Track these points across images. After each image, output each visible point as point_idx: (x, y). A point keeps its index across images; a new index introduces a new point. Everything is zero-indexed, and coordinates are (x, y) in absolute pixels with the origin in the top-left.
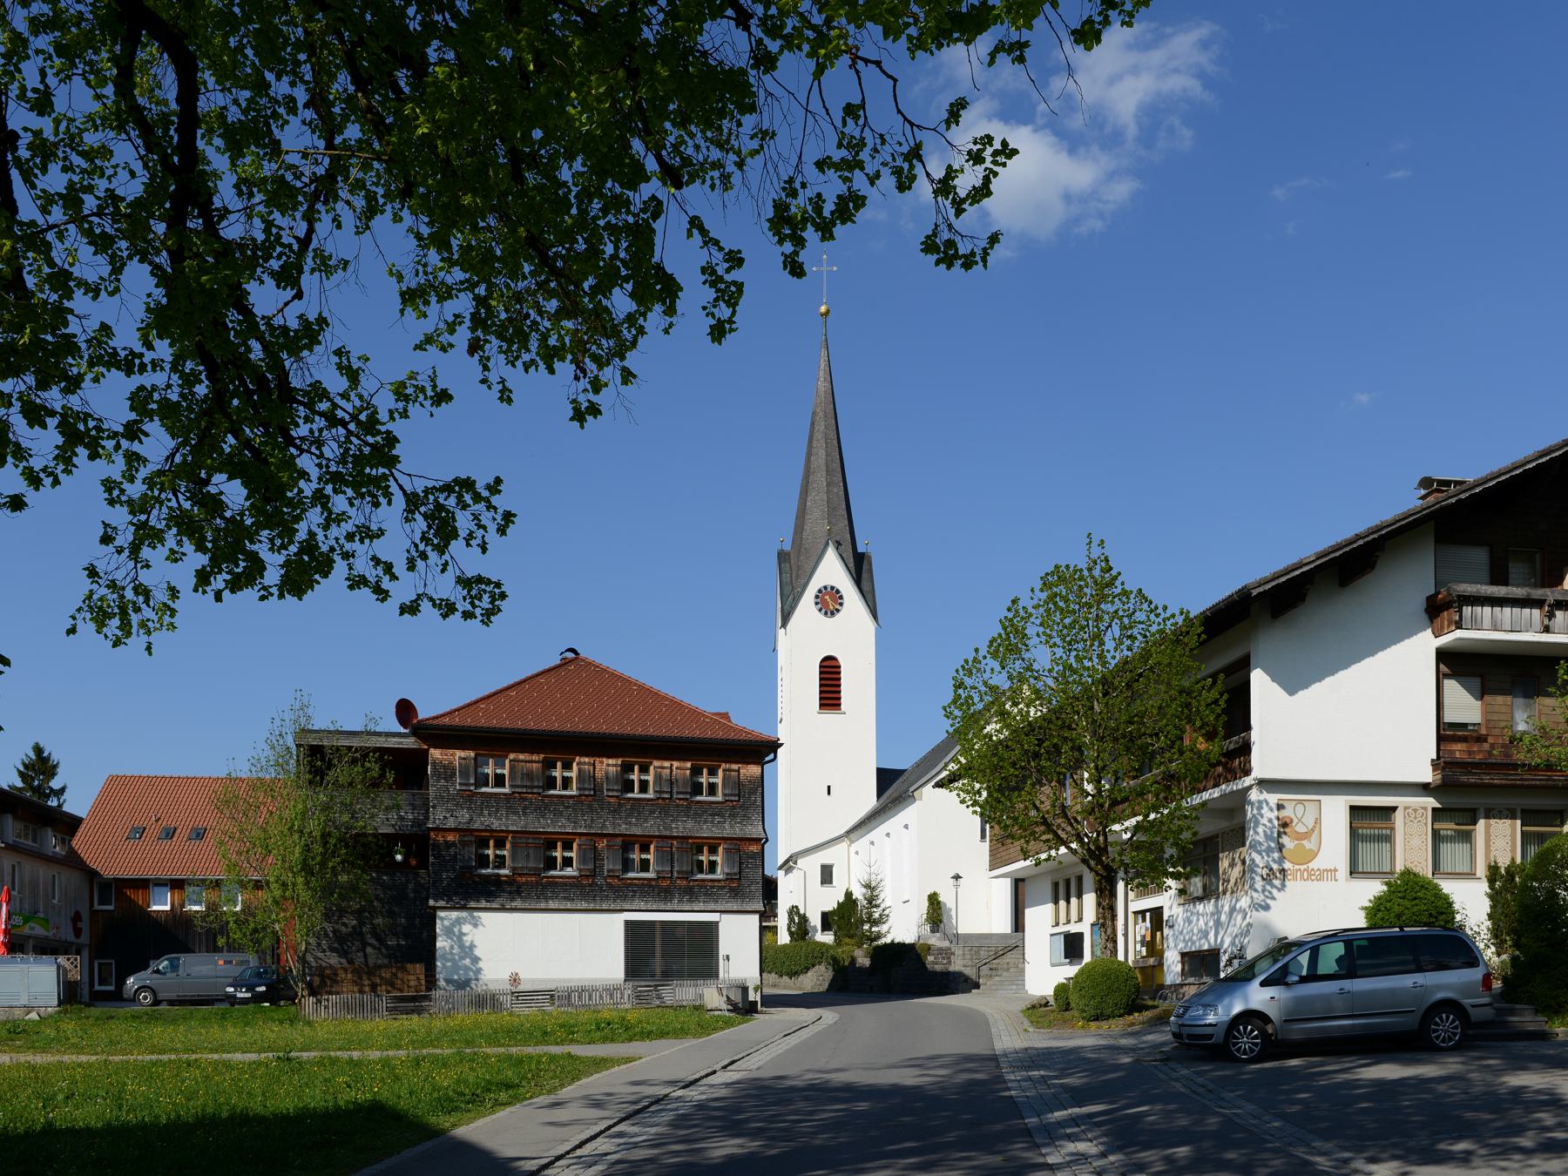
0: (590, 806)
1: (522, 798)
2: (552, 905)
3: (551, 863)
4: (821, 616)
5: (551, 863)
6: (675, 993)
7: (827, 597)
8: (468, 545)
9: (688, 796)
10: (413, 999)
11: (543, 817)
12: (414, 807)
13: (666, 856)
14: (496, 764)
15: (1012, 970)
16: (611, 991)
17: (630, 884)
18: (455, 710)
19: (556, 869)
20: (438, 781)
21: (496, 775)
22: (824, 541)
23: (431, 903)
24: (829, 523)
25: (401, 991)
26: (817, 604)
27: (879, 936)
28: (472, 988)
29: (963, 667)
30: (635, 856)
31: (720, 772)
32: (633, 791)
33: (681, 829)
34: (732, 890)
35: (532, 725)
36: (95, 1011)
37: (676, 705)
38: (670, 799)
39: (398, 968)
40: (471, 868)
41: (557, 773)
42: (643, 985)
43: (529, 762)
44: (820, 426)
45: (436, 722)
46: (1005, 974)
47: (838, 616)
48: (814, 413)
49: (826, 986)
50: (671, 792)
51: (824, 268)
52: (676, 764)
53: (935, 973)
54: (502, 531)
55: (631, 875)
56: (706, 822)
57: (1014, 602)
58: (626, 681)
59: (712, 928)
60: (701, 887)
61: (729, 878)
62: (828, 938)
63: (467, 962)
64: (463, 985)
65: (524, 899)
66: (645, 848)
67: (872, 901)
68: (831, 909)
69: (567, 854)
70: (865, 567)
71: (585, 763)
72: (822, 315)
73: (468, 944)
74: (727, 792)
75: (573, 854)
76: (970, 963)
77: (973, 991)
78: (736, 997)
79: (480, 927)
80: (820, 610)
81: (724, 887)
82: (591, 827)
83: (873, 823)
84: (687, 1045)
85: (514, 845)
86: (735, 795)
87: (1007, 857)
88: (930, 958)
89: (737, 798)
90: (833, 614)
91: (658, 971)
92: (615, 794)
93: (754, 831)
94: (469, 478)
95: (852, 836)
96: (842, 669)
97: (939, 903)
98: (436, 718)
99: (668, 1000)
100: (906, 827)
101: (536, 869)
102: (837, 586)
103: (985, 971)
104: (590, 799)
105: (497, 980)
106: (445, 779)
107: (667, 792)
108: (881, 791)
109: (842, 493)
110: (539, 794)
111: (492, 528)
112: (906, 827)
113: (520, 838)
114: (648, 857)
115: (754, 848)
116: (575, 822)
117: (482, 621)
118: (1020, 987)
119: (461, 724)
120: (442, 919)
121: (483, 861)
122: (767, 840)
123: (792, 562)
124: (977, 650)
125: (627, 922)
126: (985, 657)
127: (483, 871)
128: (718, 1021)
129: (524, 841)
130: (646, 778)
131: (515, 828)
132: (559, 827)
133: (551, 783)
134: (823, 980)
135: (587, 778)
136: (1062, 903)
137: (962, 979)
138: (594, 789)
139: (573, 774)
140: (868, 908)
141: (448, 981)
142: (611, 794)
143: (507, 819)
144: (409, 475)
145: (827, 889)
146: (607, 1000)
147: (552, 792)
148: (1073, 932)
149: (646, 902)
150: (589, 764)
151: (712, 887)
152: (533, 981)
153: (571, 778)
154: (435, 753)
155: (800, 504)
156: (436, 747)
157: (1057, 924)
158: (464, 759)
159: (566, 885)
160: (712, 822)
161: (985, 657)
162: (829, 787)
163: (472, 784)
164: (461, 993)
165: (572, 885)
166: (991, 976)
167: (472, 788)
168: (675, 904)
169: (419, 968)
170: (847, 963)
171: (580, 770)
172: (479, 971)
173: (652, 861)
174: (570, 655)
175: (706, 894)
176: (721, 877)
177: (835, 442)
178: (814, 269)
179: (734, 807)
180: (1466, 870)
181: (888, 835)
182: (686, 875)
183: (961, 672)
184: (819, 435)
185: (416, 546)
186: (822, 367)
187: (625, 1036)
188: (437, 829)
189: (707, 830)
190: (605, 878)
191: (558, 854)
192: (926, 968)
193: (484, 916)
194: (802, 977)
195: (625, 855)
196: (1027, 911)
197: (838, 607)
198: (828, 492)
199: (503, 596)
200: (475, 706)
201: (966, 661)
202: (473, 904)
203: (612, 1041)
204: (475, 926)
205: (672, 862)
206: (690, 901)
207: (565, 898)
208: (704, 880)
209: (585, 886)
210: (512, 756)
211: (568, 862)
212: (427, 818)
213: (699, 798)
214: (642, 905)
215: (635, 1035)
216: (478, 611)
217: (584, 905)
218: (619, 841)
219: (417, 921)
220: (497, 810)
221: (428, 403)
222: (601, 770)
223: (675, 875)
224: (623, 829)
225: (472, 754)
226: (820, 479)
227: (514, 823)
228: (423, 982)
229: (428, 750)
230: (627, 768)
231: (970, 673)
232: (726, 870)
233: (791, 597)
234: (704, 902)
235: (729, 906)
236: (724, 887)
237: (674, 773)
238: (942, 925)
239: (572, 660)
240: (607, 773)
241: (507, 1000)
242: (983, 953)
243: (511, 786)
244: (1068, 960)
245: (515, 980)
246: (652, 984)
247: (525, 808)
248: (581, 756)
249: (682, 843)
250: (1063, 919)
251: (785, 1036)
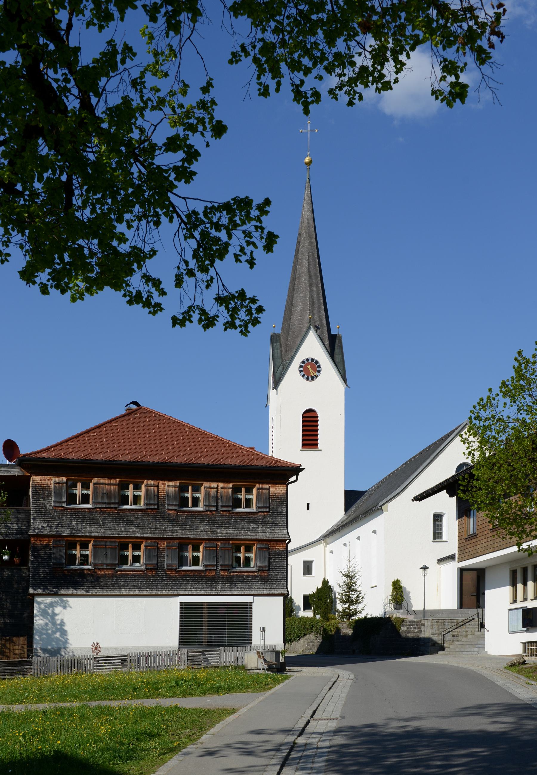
0: (155, 517)
1: (102, 512)
2: (124, 591)
3: (123, 560)
4: (303, 380)
5: (123, 560)
6: (220, 657)
7: (309, 367)
8: (238, 260)
9: (230, 509)
10: (20, 663)
11: (118, 525)
12: (18, 519)
13: (213, 554)
14: (82, 487)
15: (469, 636)
16: (170, 656)
17: (184, 575)
18: (51, 447)
19: (127, 564)
20: (38, 499)
21: (82, 494)
22: (306, 326)
23: (31, 591)
24: (311, 313)
25: (8, 657)
26: (301, 371)
27: (355, 613)
28: (61, 655)
29: (479, 403)
30: (188, 554)
31: (255, 491)
32: (187, 506)
33: (224, 534)
34: (263, 578)
35: (111, 457)
36: (215, 709)
37: (219, 442)
38: (216, 511)
39: (7, 641)
40: (62, 564)
41: (130, 493)
42: (194, 652)
43: (108, 484)
44: (305, 244)
45: (37, 456)
46: (464, 640)
47: (317, 380)
48: (300, 235)
49: (315, 650)
50: (217, 506)
51: (309, 130)
52: (221, 485)
53: (407, 639)
54: (269, 248)
55: (185, 568)
56: (243, 528)
57: (520, 353)
58: (180, 425)
59: (248, 607)
60: (239, 577)
61: (261, 570)
62: (309, 614)
63: (58, 635)
64: (55, 652)
65: (102, 587)
66: (196, 549)
67: (350, 586)
68: (311, 593)
69: (136, 553)
70: (337, 344)
71: (151, 485)
72: (306, 164)
73: (58, 622)
74: (260, 505)
75: (141, 554)
76: (437, 632)
77: (439, 652)
78: (270, 658)
79: (68, 608)
80: (303, 376)
81: (256, 577)
82: (154, 533)
83: (346, 530)
84: (262, 698)
85: (95, 547)
86: (266, 508)
87: (475, 552)
88: (404, 628)
89: (267, 510)
90: (313, 379)
91: (205, 639)
92: (174, 507)
93: (278, 534)
94: (247, 197)
95: (328, 540)
96: (319, 418)
97: (401, 587)
98: (38, 452)
99: (213, 662)
100: (375, 532)
101: (112, 564)
102: (316, 358)
103: (448, 637)
104: (155, 511)
105: (81, 649)
106: (43, 498)
107: (214, 506)
108: (348, 506)
109: (320, 291)
110: (115, 508)
111: (261, 244)
112: (375, 532)
113: (100, 541)
114: (199, 554)
115: (280, 547)
116: (143, 529)
117: (241, 332)
118: (481, 649)
119: (57, 456)
120: (39, 603)
121: (72, 559)
122: (290, 541)
123: (282, 341)
124: (490, 390)
125: (181, 604)
126: (497, 395)
127: (72, 567)
128: (267, 679)
129: (103, 543)
130: (197, 495)
131: (96, 534)
132: (131, 533)
133: (124, 500)
134: (313, 645)
135: (152, 496)
136: (520, 586)
137: (430, 644)
138: (158, 505)
139: (142, 493)
140: (347, 592)
141: (44, 650)
142: (170, 508)
143: (90, 527)
144: (184, 198)
145: (308, 579)
146: (167, 662)
147: (125, 507)
148: (529, 607)
149: (197, 588)
150: (154, 485)
151: (248, 577)
152: (108, 649)
153: (140, 496)
154: (36, 479)
156: (36, 474)
157: (515, 601)
158: (58, 483)
159: (135, 576)
160: (248, 528)
161: (497, 395)
162: (308, 504)
163: (64, 502)
164: (54, 659)
165: (140, 577)
166: (453, 641)
167: (64, 505)
168: (219, 591)
169: (23, 640)
170: (333, 633)
171: (147, 490)
172: (66, 642)
173: (201, 558)
174: (134, 407)
175: (243, 582)
176: (254, 569)
177: (316, 255)
178: (301, 131)
179: (265, 517)
180: (465, 573)
181: (359, 538)
182: (228, 568)
183: (478, 408)
184: (303, 250)
185: (186, 263)
186: (306, 201)
187: (199, 690)
188: (36, 536)
189: (244, 534)
190: (165, 571)
191: (129, 553)
192: (401, 636)
193: (71, 601)
194: (294, 644)
195: (181, 553)
196: (487, 592)
198: (310, 291)
199: (260, 310)
200: (66, 444)
201: (482, 400)
202: (63, 592)
203: (190, 694)
204: (65, 607)
205: (217, 557)
206: (231, 587)
207: (134, 586)
208: (241, 572)
209: (149, 577)
210: (95, 480)
211: (136, 559)
212: (29, 527)
213: (238, 510)
214: (194, 591)
215: (208, 690)
216: (238, 322)
217: (149, 591)
218: (176, 543)
219: (20, 604)
220: (83, 521)
221: (208, 134)
222: (163, 490)
223: (219, 567)
224: (180, 534)
225: (65, 479)
226: (304, 281)
227: (97, 530)
228: (26, 651)
229: (29, 477)
230: (183, 489)
231: (484, 407)
232: (259, 564)
233: (281, 368)
235: (261, 591)
236: (256, 577)
237: (220, 491)
238: (404, 603)
239: (136, 410)
240: (168, 492)
241: (90, 666)
242: (447, 624)
243: (94, 503)
244: (525, 629)
245: (96, 648)
246: (201, 650)
247: (104, 519)
248: (148, 479)
249: (225, 544)
250: (520, 596)
251: (330, 689)
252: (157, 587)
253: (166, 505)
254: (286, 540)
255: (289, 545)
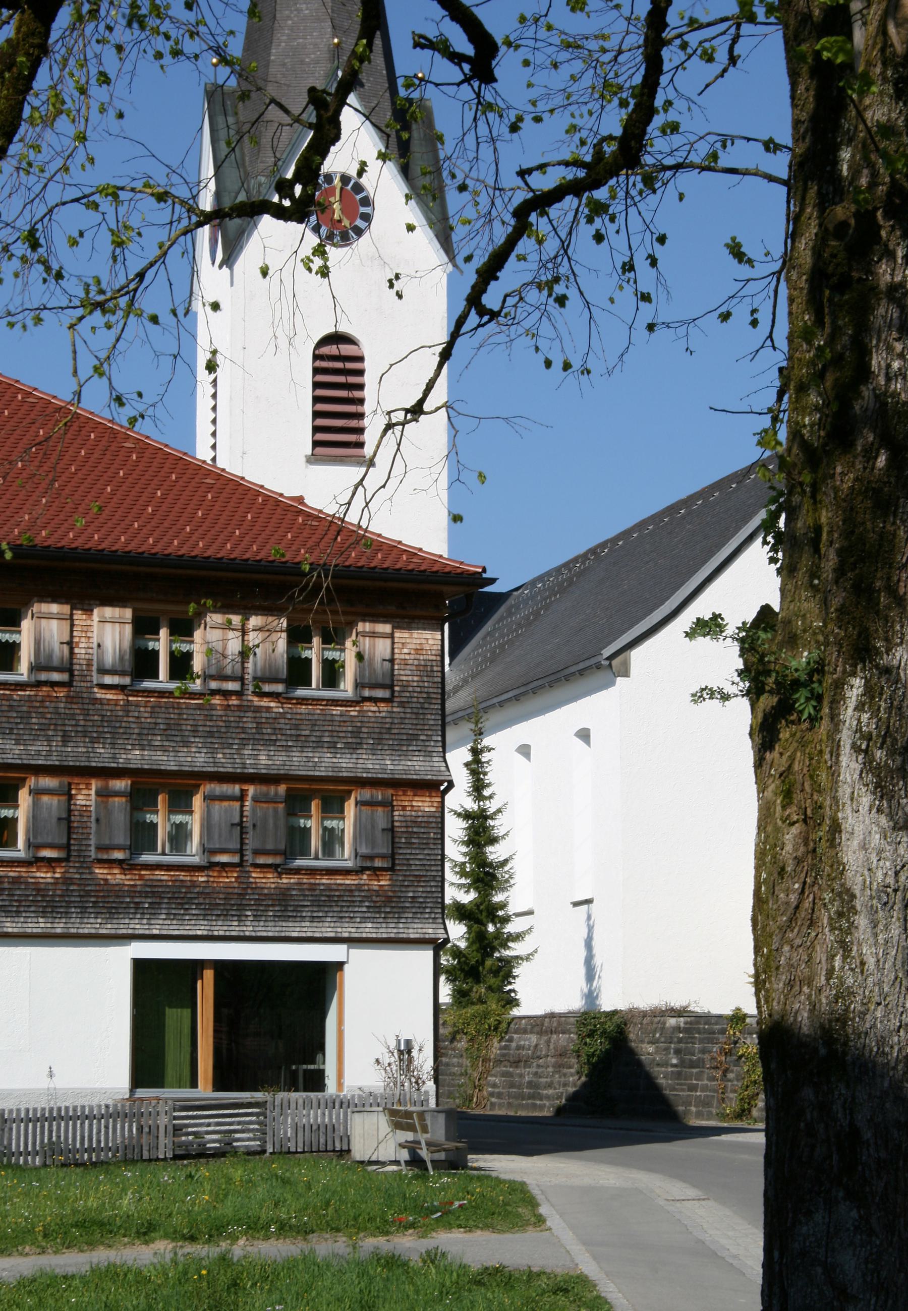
130: (185, 648)
155: (775, 177)
197: (359, 223)
217: (40, 925)
223: (249, 857)
232: (363, 850)
234: (313, 919)
235: (368, 930)
252: (241, 918)
253: (94, 674)
254: (441, 783)
255: (447, 797)
